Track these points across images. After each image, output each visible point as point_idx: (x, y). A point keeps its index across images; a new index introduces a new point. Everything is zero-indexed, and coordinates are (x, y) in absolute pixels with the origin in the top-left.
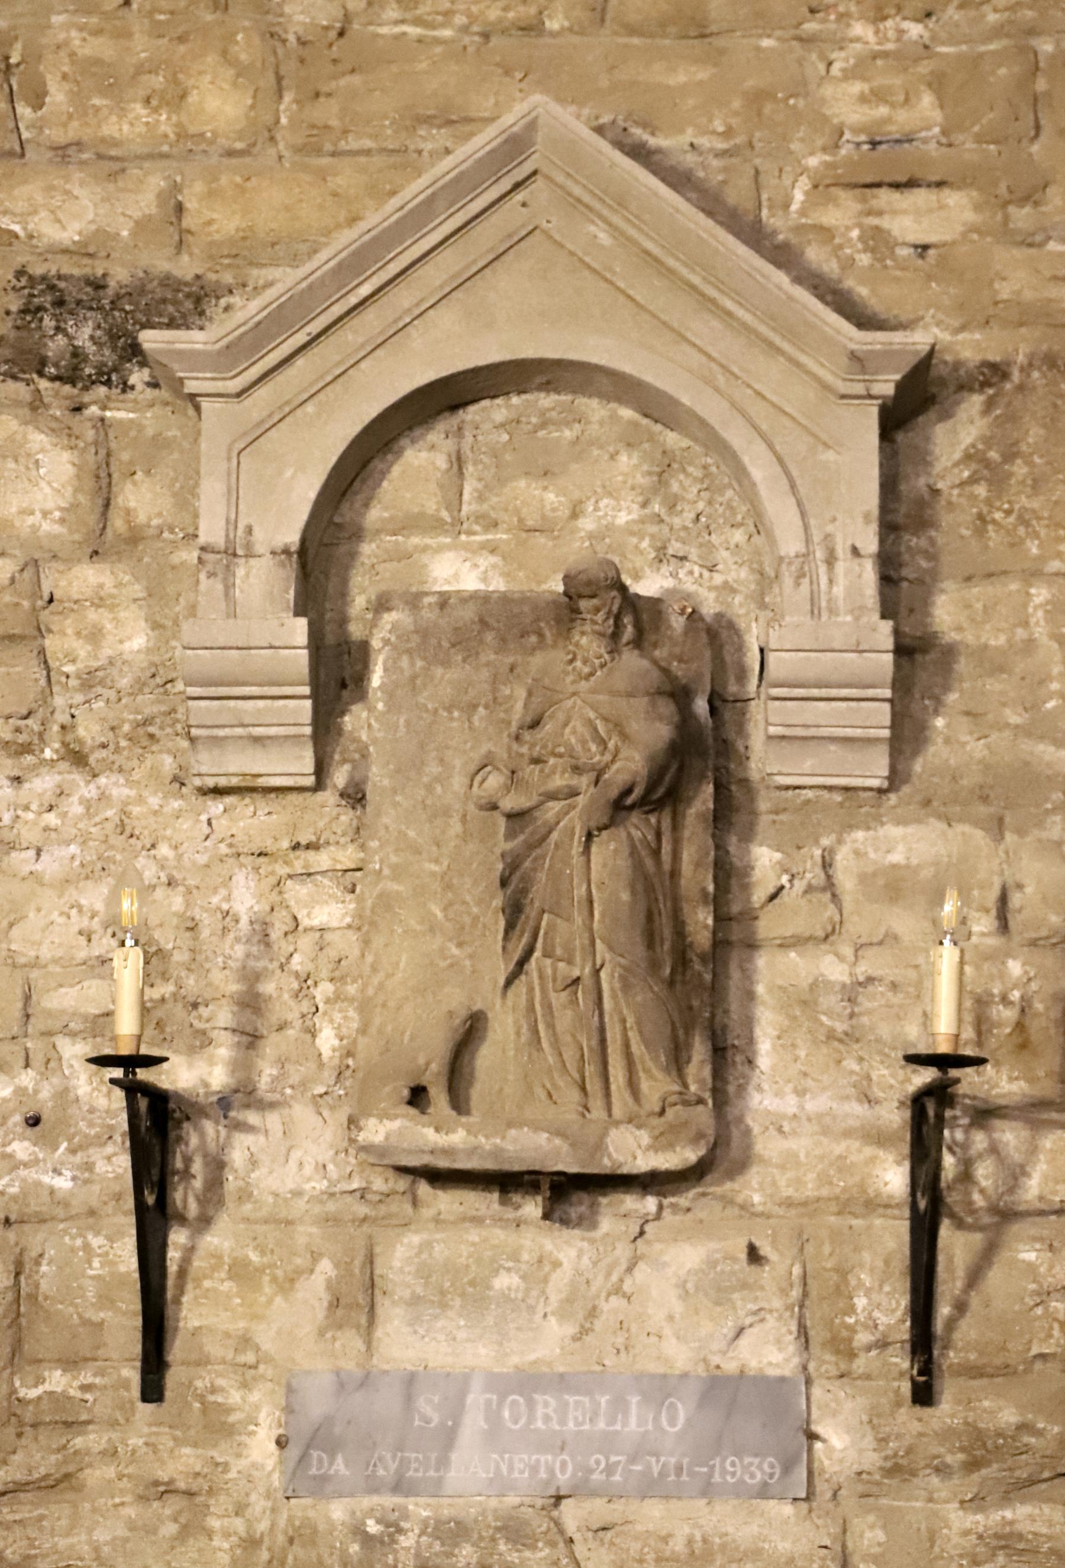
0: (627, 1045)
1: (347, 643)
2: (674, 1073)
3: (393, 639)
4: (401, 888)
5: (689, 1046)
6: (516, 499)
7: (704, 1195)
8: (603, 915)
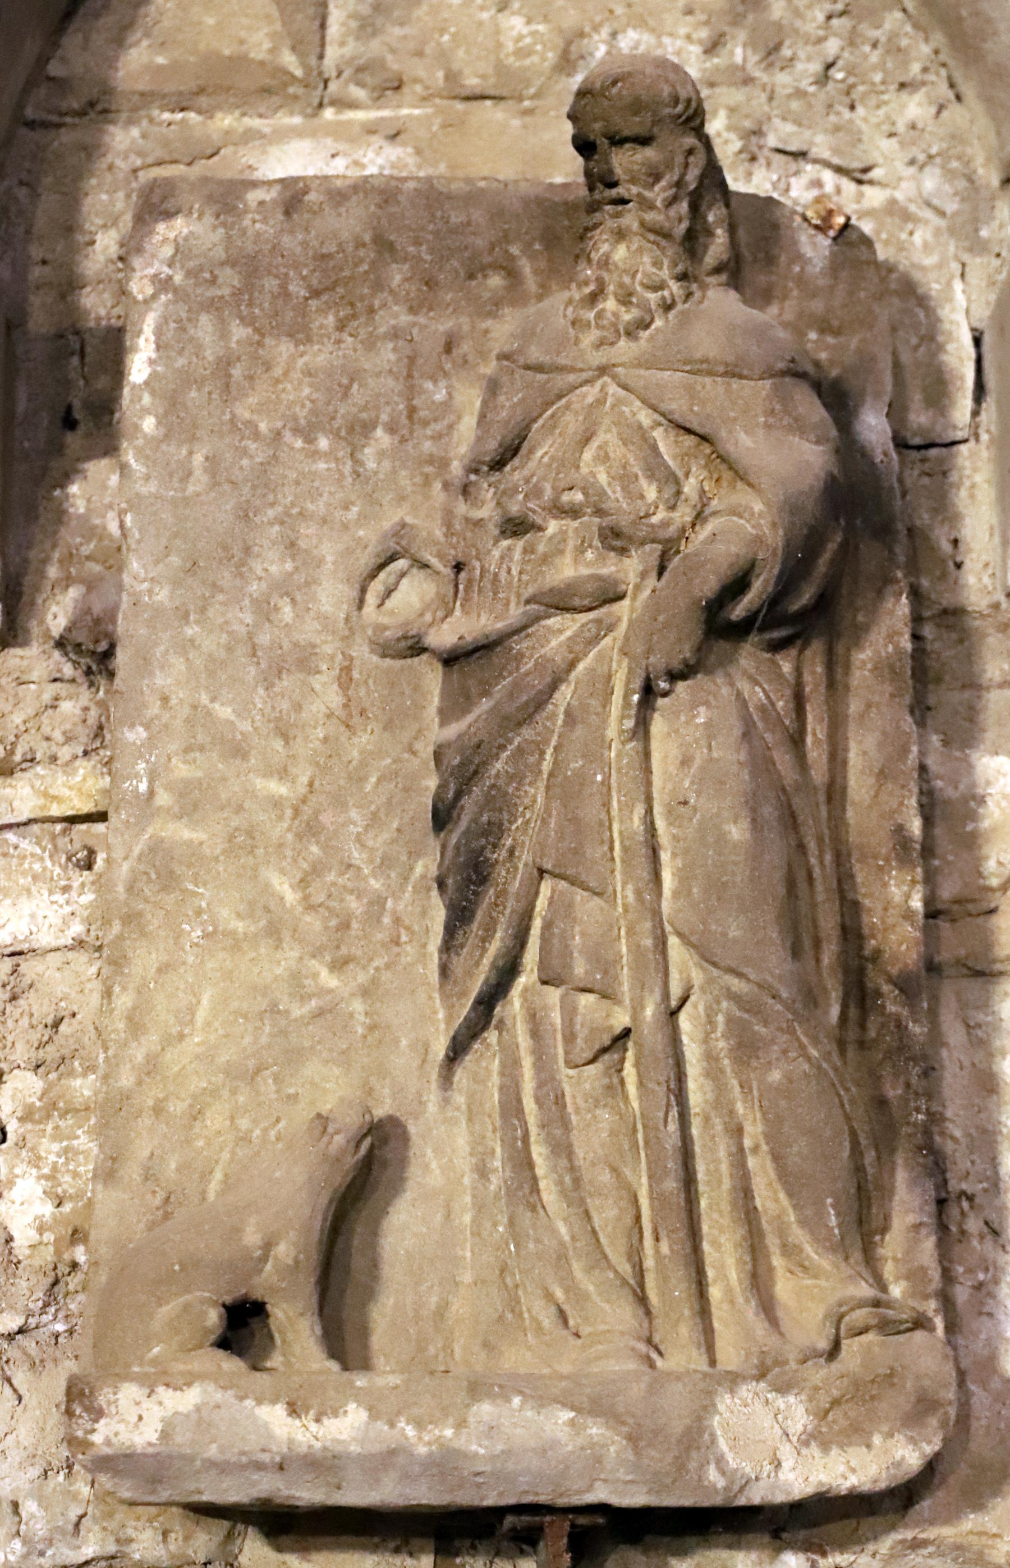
0: (744, 1192)
1: (77, 333)
2: (857, 1256)
3: (178, 279)
4: (197, 835)
5: (887, 1192)
6: (442, 31)
7: (916, 1545)
8: (684, 878)
